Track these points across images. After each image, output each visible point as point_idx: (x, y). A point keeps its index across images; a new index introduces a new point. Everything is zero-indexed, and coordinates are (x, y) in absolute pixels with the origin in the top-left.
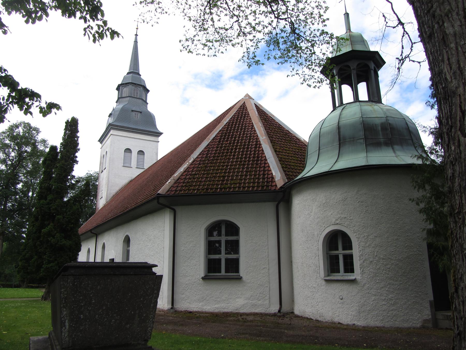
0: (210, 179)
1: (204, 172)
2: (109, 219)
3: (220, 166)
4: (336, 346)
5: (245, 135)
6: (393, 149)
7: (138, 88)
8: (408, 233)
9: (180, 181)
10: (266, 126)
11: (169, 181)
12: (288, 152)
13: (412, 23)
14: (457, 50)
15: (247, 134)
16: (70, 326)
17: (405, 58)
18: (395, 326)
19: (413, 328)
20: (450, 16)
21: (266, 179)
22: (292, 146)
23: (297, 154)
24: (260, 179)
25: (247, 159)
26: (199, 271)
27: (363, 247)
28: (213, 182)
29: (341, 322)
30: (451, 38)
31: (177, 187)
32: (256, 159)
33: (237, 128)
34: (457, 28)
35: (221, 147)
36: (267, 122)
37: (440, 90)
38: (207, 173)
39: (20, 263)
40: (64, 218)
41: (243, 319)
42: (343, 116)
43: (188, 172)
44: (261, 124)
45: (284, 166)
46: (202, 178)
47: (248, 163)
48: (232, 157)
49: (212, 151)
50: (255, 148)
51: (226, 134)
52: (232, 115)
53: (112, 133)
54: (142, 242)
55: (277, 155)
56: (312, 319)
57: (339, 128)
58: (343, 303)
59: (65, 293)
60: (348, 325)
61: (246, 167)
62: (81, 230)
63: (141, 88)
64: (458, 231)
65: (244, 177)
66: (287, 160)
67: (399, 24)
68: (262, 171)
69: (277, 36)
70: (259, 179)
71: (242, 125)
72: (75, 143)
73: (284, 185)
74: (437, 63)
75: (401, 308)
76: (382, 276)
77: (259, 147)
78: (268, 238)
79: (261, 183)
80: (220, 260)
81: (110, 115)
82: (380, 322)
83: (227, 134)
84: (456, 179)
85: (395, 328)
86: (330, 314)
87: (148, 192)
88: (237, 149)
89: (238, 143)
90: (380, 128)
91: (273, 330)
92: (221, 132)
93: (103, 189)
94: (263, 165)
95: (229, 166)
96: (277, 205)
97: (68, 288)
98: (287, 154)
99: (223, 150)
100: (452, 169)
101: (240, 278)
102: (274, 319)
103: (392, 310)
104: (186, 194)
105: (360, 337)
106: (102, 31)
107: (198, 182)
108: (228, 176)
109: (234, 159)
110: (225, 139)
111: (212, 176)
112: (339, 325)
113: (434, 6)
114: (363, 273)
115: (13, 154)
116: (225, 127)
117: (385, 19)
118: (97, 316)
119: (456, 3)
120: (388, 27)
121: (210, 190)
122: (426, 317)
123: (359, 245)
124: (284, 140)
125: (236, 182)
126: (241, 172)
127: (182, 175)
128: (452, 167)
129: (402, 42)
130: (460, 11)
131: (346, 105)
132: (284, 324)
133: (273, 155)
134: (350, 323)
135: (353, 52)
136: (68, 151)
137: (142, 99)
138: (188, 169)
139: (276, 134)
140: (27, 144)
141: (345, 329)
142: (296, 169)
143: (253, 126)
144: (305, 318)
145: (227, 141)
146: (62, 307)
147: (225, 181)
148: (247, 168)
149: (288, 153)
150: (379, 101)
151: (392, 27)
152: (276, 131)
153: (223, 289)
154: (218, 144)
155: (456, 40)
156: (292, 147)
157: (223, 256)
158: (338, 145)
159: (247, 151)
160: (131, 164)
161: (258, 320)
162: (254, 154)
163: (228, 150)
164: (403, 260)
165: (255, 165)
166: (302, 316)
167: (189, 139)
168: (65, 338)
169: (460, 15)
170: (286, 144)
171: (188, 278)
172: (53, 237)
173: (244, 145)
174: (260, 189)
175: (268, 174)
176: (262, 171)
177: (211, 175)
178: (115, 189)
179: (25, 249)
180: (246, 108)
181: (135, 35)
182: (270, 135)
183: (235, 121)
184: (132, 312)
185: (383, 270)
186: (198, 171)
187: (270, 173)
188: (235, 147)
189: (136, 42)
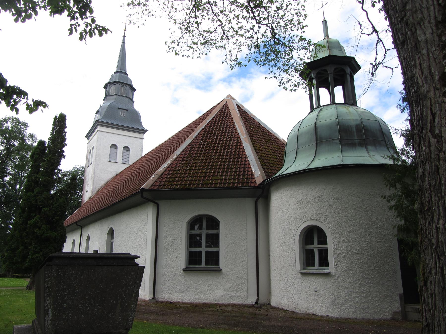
1: (187, 168)
2: (94, 212)
3: (202, 163)
5: (227, 134)
6: (367, 149)
9: (163, 176)
11: (153, 176)
12: (267, 150)
15: (228, 133)
16: (53, 315)
18: (366, 318)
20: (422, 24)
21: (246, 176)
22: (271, 145)
23: (276, 152)
24: (241, 175)
27: (337, 242)
28: (195, 178)
29: (315, 313)
30: (423, 45)
31: (161, 182)
32: (237, 156)
33: (219, 127)
34: (429, 36)
35: (204, 145)
36: (248, 121)
37: (412, 94)
40: (50, 210)
41: (221, 309)
42: (320, 117)
43: (172, 167)
44: (242, 123)
46: (185, 174)
48: (214, 154)
49: (195, 148)
50: (237, 146)
51: (208, 132)
52: (215, 115)
53: (99, 130)
55: (257, 153)
57: (316, 128)
58: (317, 295)
59: (49, 282)
60: (322, 317)
62: (67, 222)
63: (128, 87)
64: (427, 227)
65: (225, 174)
66: (266, 158)
67: (373, 31)
68: (242, 168)
70: (239, 175)
71: (224, 124)
73: (263, 182)
74: (409, 68)
75: (373, 301)
77: (240, 146)
78: (247, 232)
79: (241, 180)
80: (200, 253)
81: (97, 112)
82: (352, 314)
83: (209, 132)
85: (366, 319)
86: (305, 306)
89: (219, 141)
90: (354, 129)
92: (204, 130)
94: (243, 162)
97: (52, 278)
99: (206, 147)
100: (423, 168)
101: (219, 271)
102: (251, 310)
103: (364, 303)
104: (169, 188)
107: (181, 177)
108: (210, 173)
109: (216, 156)
111: (194, 172)
112: (313, 317)
113: (407, 14)
114: (337, 266)
116: (208, 125)
117: (361, 26)
118: (80, 305)
119: (428, 12)
120: (363, 34)
121: (193, 185)
123: (334, 240)
124: (264, 139)
125: (217, 178)
126: (222, 169)
127: (165, 171)
130: (431, 20)
131: (322, 107)
133: (253, 153)
134: (324, 315)
135: (330, 57)
136: (56, 146)
137: (129, 98)
139: (256, 133)
140: (16, 138)
141: (319, 320)
142: (275, 167)
143: (234, 125)
144: (281, 309)
145: (209, 139)
146: (46, 296)
147: (207, 177)
148: (228, 165)
151: (367, 34)
152: (257, 131)
153: (202, 281)
154: (201, 142)
156: (271, 146)
157: (204, 249)
158: (315, 145)
160: (116, 160)
162: (235, 152)
163: (210, 147)
165: (236, 162)
168: (48, 326)
169: (431, 23)
170: (266, 143)
171: (170, 270)
172: (39, 228)
173: (226, 143)
174: (240, 185)
175: (248, 171)
176: (242, 168)
177: (193, 171)
179: (11, 240)
180: (228, 108)
181: (123, 36)
182: (250, 134)
183: (217, 120)
184: (115, 302)
185: (356, 264)
186: (181, 167)
187: (250, 170)
189: (124, 43)
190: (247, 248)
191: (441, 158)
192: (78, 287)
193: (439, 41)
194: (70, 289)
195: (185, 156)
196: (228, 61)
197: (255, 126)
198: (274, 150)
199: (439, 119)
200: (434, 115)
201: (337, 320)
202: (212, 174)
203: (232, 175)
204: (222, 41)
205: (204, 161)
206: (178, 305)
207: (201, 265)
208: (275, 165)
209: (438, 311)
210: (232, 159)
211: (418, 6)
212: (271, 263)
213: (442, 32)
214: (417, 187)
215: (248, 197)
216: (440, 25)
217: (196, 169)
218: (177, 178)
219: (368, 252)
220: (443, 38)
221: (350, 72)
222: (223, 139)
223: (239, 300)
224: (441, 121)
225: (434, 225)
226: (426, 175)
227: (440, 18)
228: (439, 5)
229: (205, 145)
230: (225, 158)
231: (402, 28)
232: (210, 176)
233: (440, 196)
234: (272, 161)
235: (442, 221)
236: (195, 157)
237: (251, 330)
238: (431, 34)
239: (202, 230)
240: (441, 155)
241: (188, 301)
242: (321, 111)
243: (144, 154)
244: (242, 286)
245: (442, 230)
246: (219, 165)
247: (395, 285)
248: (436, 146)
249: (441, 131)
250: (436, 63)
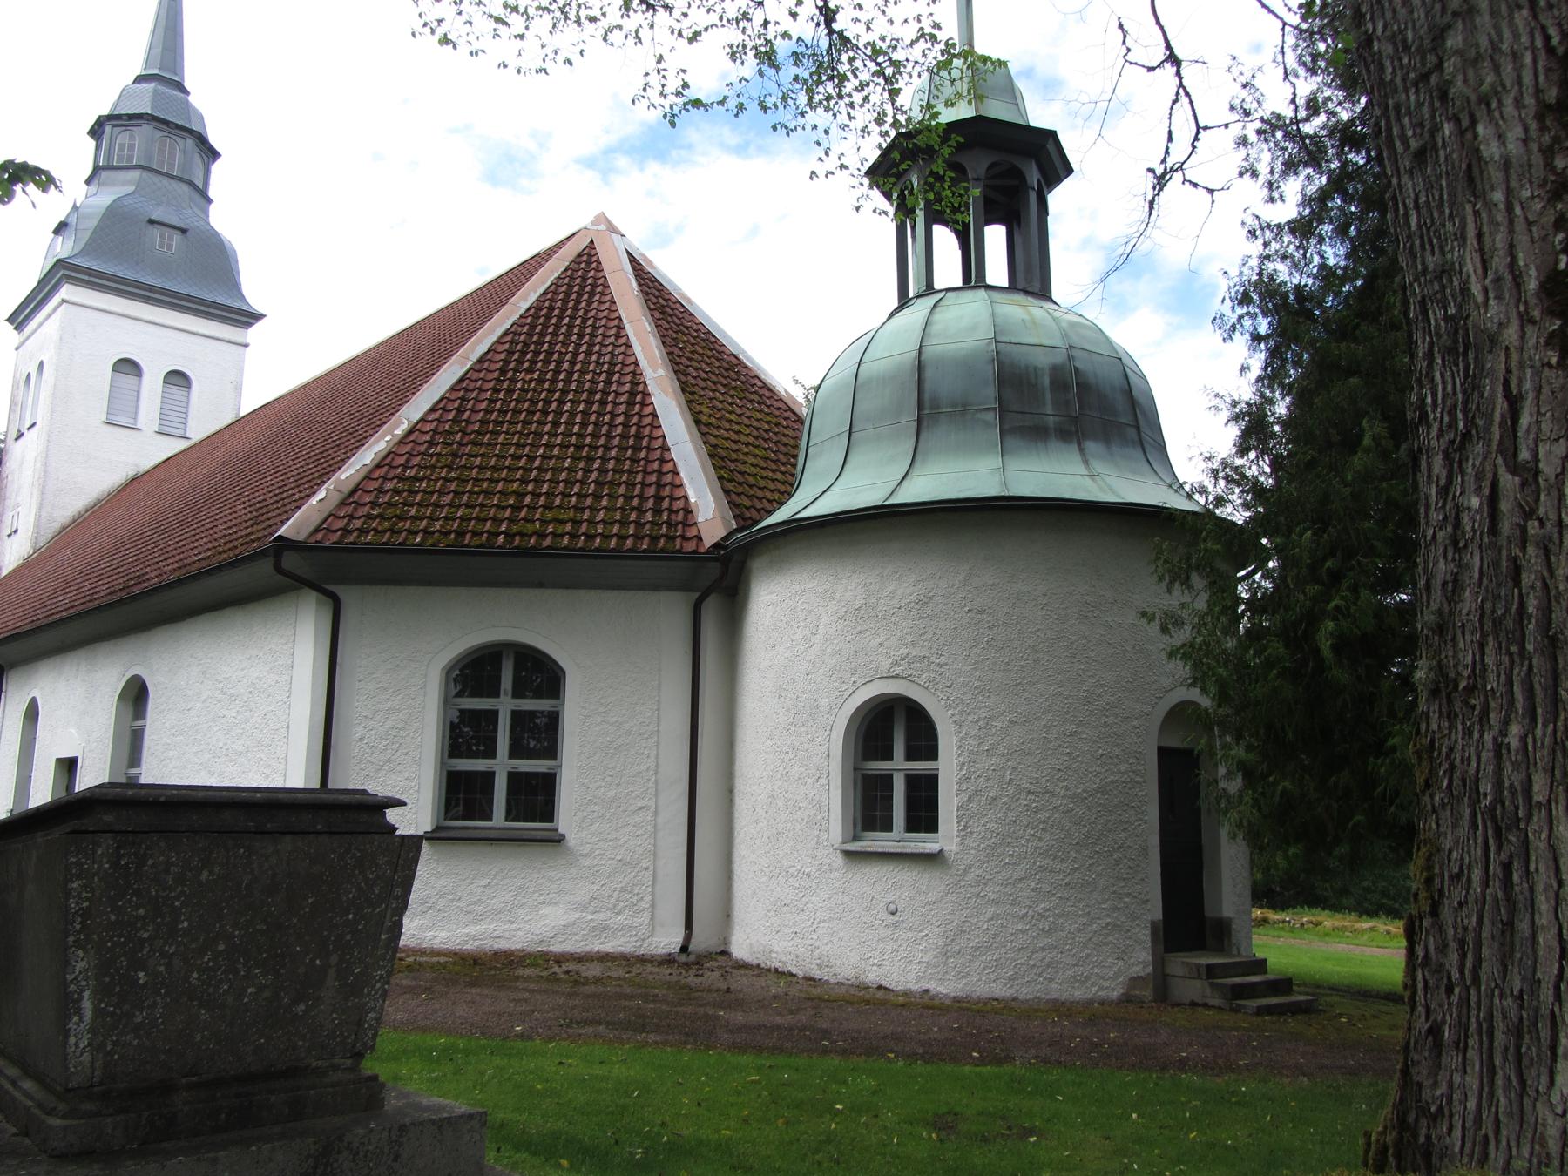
0: (469, 498)
1: (448, 472)
2: (64, 614)
3: (505, 457)
4: (889, 1060)
6: (1082, 450)
7: (175, 137)
8: (1107, 717)
9: (360, 497)
10: (665, 333)
11: (321, 494)
12: (736, 428)
13: (1204, 63)
14: (1510, 213)
15: (600, 355)
16: (98, 1012)
17: (1172, 170)
18: (1048, 997)
19: (1099, 1003)
20: (1494, 105)
21: (666, 513)
22: (748, 409)
23: (766, 436)
24: (647, 511)
25: (602, 442)
26: (415, 813)
27: (971, 752)
28: (481, 511)
29: (886, 984)
30: (1496, 175)
31: (351, 517)
32: (631, 441)
33: (567, 331)
34: (1513, 147)
36: (669, 319)
37: (1433, 322)
38: (458, 479)
41: (567, 972)
42: (935, 329)
43: (391, 467)
44: (650, 324)
45: (725, 476)
46: (441, 493)
47: (604, 454)
48: (547, 428)
49: (477, 400)
50: (630, 404)
52: (549, 283)
53: (66, 297)
54: (199, 705)
55: (703, 434)
56: (795, 975)
57: (920, 366)
58: (895, 925)
59: (84, 894)
60: (906, 994)
61: (596, 465)
63: (190, 142)
64: (1456, 741)
65: (589, 502)
66: (734, 456)
67: (1166, 60)
68: (650, 485)
69: (766, 29)
70: (641, 511)
71: (585, 320)
73: (725, 538)
74: (1435, 241)
75: (1070, 944)
76: (1023, 845)
77: (643, 404)
78: (658, 710)
79: (648, 526)
80: (489, 776)
81: (61, 228)
82: (1005, 985)
83: (529, 345)
84: (1463, 590)
85: (1048, 1001)
86: (854, 958)
87: (230, 528)
88: (565, 403)
89: (568, 381)
90: (1047, 381)
91: (680, 1009)
92: (509, 338)
93: (19, 499)
94: (656, 465)
95: (539, 459)
96: (697, 599)
97: (96, 879)
98: (732, 433)
99: (517, 401)
100: (1454, 560)
101: (557, 840)
102: (671, 974)
103: (1043, 949)
104: (384, 544)
105: (952, 1029)
107: (427, 506)
109: (556, 435)
110: (524, 362)
111: (476, 489)
112: (880, 995)
113: (1446, 65)
114: (965, 833)
116: (523, 320)
117: (1125, 37)
118: (195, 975)
119: (1515, 69)
120: (1131, 63)
121: (471, 538)
122: (1136, 969)
123: (960, 747)
124: (725, 386)
125: (561, 517)
126: (578, 484)
127: (367, 478)
128: (1454, 554)
129: (1170, 118)
130: (1525, 95)
131: (941, 295)
132: (709, 991)
133: (691, 434)
134: (913, 987)
135: (979, 121)
137: (191, 184)
138: (389, 459)
139: (698, 362)
141: (903, 1005)
143: (621, 328)
144: (769, 970)
145: (530, 371)
146: (71, 943)
147: (525, 509)
150: (1042, 292)
151: (1143, 66)
152: (699, 354)
153: (495, 876)
154: (497, 380)
155: (1507, 181)
156: (748, 413)
157: (502, 765)
158: (916, 423)
160: (135, 419)
161: (620, 979)
162: (626, 425)
163: (534, 402)
164: (1086, 798)
165: (628, 462)
166: (758, 966)
167: (374, 348)
168: (78, 1054)
169: (1524, 107)
170: (730, 400)
173: (592, 392)
174: (645, 547)
175: (672, 498)
176: (650, 485)
177: (474, 486)
180: (599, 263)
182: (677, 364)
183: (559, 304)
184: (318, 962)
185: (1027, 826)
186: (426, 467)
187: (678, 493)
188: (557, 394)
191: (1533, 536)
192: (190, 909)
193: (1545, 169)
194: (159, 920)
195: (440, 430)
196: (653, 93)
197: (694, 338)
198: (757, 429)
199: (1531, 415)
200: (1516, 402)
201: (958, 1005)
202: (542, 500)
203: (616, 510)
204: (628, 16)
205: (512, 451)
206: (411, 959)
208: (762, 483)
209: (1486, 989)
210: (616, 449)
211: (1484, 42)
212: (736, 815)
213: (1556, 140)
214: (1432, 617)
215: (669, 588)
216: (1551, 118)
217: (482, 480)
218: (412, 505)
219: (1067, 790)
220: (1560, 163)
221: (1039, 181)
222: (579, 376)
223: (623, 940)
224: (1538, 422)
225: (1486, 736)
226: (1464, 582)
227: (1552, 95)
228: (1550, 50)
229: (514, 391)
230: (590, 446)
231: (1420, 105)
232: (534, 508)
233: (1517, 651)
235: (1520, 726)
236: (478, 432)
237: (691, 1040)
238: (1519, 142)
239: (498, 695)
240: (1533, 528)
241: (441, 943)
242: (938, 310)
244: (636, 892)
245: (1517, 752)
246: (567, 468)
247: (1140, 893)
248: (1516, 498)
249: (1537, 454)
250: (1532, 237)
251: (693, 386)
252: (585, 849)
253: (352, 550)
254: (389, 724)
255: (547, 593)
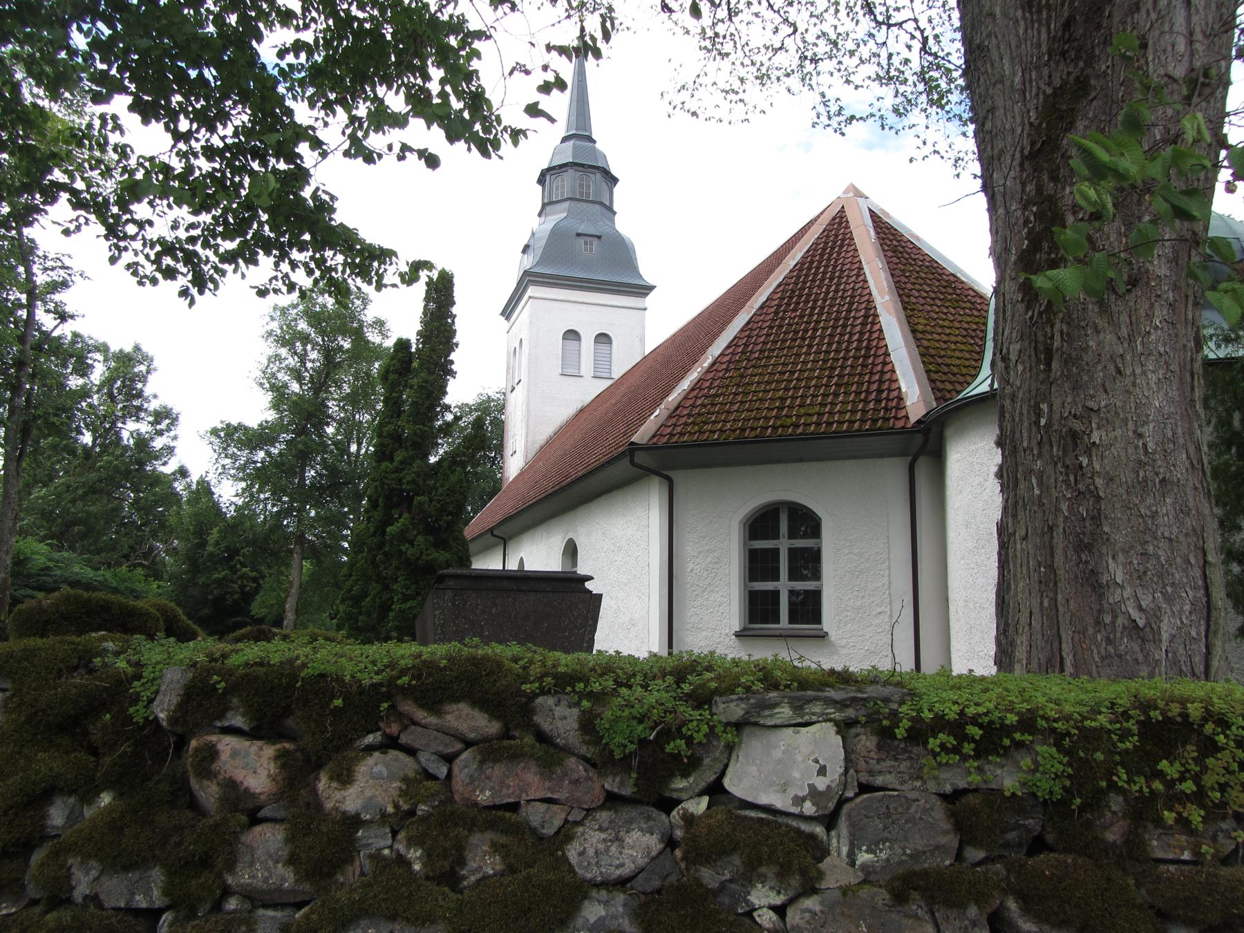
3: (775, 374)
5: (840, 294)
15: (845, 291)
23: (973, 334)
31: (675, 425)
32: (863, 352)
35: (780, 326)
39: (341, 609)
40: (431, 501)
43: (701, 389)
46: (732, 403)
47: (843, 363)
48: (804, 350)
49: (758, 336)
50: (864, 324)
51: (793, 291)
53: (531, 295)
62: (469, 531)
63: (598, 175)
65: (830, 399)
66: (943, 353)
70: (866, 401)
72: (448, 331)
79: (871, 412)
81: (526, 249)
89: (820, 314)
92: (781, 288)
94: (879, 368)
99: (785, 333)
101: (823, 636)
106: (496, 134)
108: (794, 398)
109: (810, 354)
115: (314, 355)
124: (941, 300)
127: (686, 398)
133: (906, 341)
136: (434, 350)
137: (602, 204)
139: (921, 285)
140: (345, 332)
142: (963, 375)
143: (860, 268)
145: (794, 310)
148: (841, 376)
149: (946, 335)
152: (922, 279)
154: (773, 320)
157: (784, 585)
159: (841, 335)
163: (796, 332)
165: (859, 368)
170: (945, 311)
171: (704, 633)
172: (411, 543)
178: (545, 431)
179: (350, 575)
182: (903, 289)
187: (894, 386)
190: (890, 583)
197: (920, 266)
198: (966, 330)
202: (798, 402)
207: (779, 623)
228: (1031, 124)
230: (833, 359)
234: (958, 358)
236: (758, 359)
243: (649, 349)
251: (914, 304)
252: (843, 642)
253: (677, 446)
254: (709, 560)
255: (806, 465)
